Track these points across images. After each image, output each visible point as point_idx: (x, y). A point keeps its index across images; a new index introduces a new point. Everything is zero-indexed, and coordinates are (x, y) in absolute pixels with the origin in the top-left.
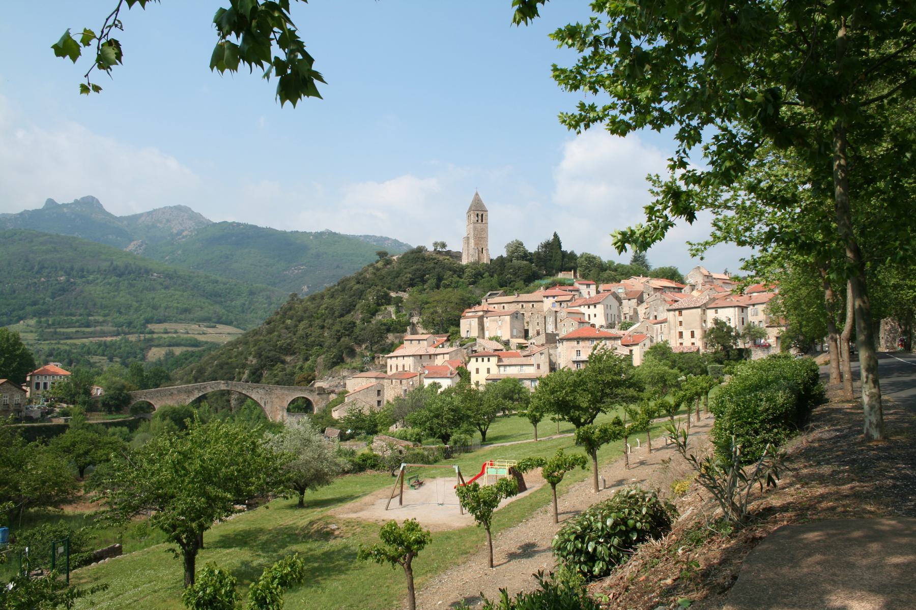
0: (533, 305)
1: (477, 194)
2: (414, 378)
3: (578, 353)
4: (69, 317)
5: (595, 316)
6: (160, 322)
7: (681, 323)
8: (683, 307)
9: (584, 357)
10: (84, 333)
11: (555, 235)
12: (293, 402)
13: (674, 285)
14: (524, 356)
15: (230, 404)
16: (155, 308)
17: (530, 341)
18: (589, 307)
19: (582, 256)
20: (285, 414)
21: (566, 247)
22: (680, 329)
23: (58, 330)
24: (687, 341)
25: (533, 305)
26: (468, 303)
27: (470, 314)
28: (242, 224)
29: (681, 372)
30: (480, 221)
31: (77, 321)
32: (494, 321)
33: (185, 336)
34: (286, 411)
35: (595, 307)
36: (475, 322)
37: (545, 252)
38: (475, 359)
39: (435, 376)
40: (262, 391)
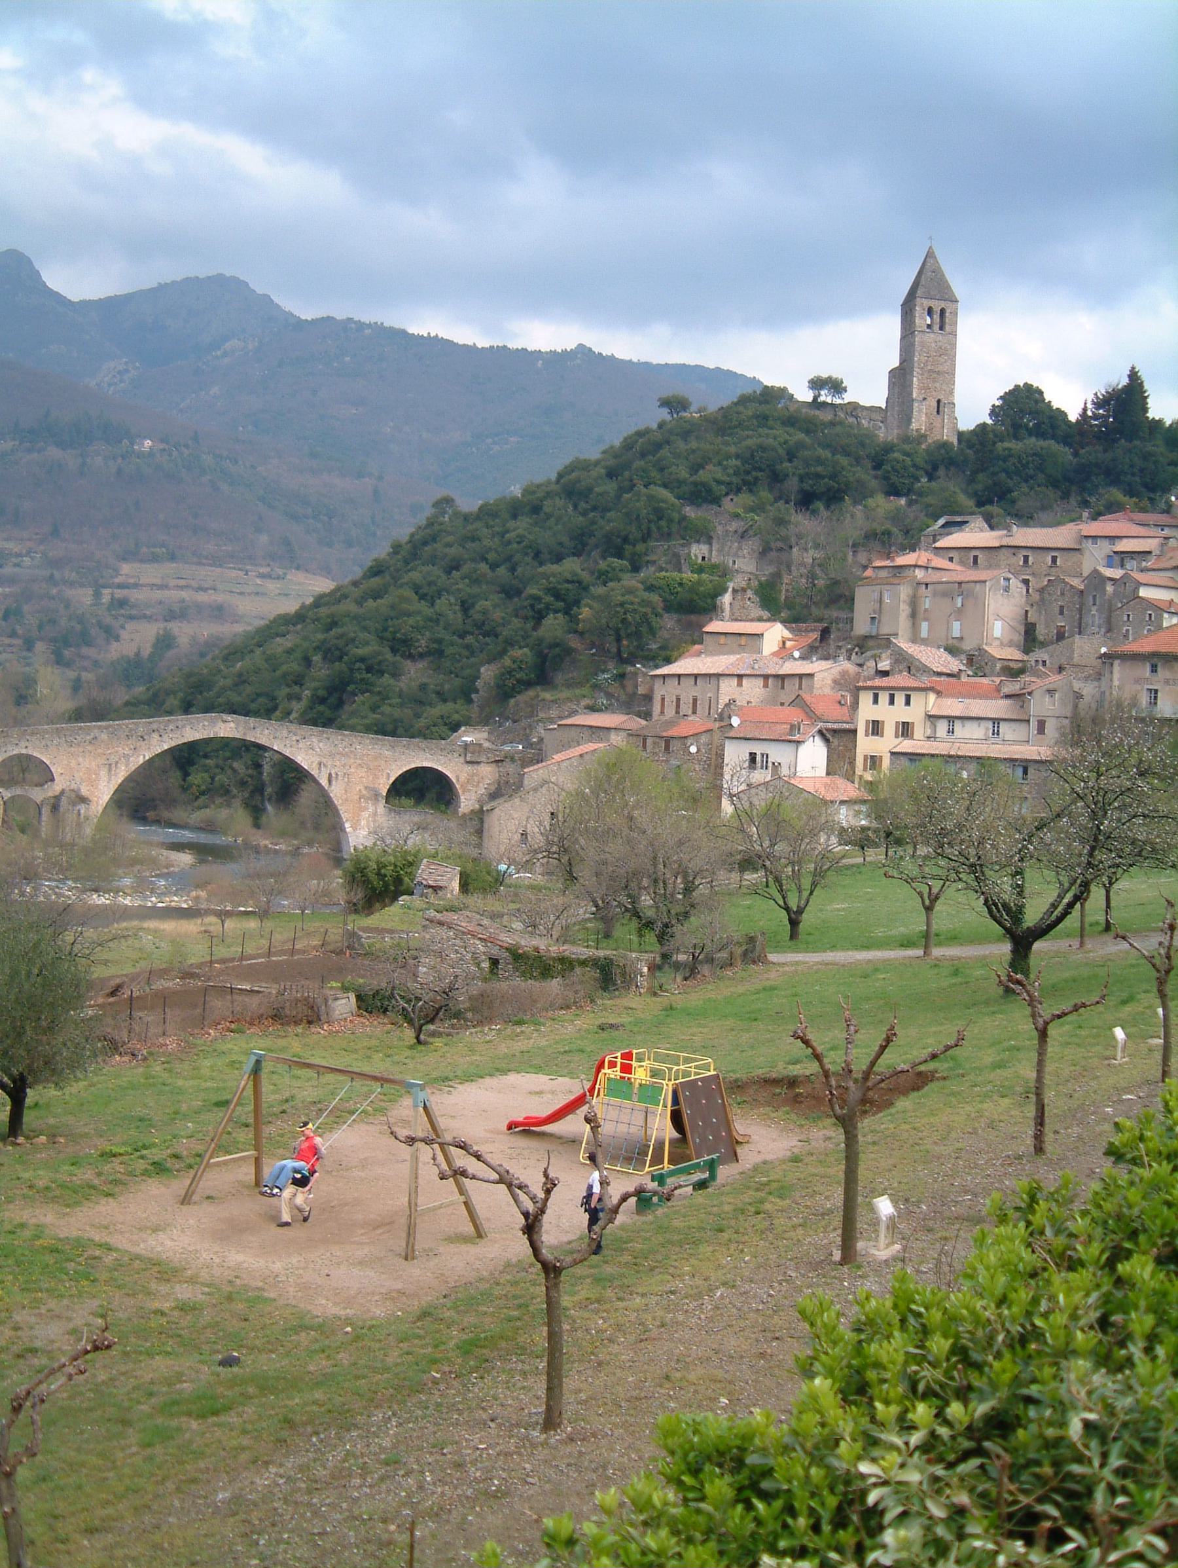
0: (1054, 559)
1: (930, 255)
2: (704, 739)
11: (1133, 375)
15: (261, 773)
20: (381, 807)
25: (1054, 559)
30: (936, 327)
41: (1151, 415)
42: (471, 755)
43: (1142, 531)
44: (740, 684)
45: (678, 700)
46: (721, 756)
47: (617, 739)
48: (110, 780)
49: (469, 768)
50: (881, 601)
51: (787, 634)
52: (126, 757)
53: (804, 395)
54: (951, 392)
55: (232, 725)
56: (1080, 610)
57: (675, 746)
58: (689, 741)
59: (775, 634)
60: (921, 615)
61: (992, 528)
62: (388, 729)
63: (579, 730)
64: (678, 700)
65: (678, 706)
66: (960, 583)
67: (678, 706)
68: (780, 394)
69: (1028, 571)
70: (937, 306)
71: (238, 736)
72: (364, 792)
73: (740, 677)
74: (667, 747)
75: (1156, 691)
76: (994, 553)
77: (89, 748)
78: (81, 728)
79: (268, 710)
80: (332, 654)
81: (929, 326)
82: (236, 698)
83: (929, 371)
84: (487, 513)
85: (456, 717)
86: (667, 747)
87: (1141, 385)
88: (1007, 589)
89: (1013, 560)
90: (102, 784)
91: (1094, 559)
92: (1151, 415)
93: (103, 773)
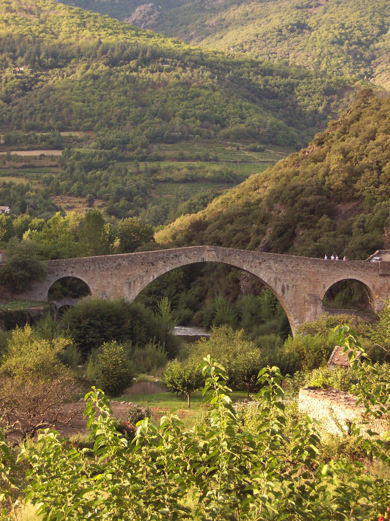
4: (31, 132)
6: (173, 140)
12: (51, 291)
16: (166, 117)
23: (13, 153)
29: (313, 335)
31: (44, 139)
40: (276, 267)
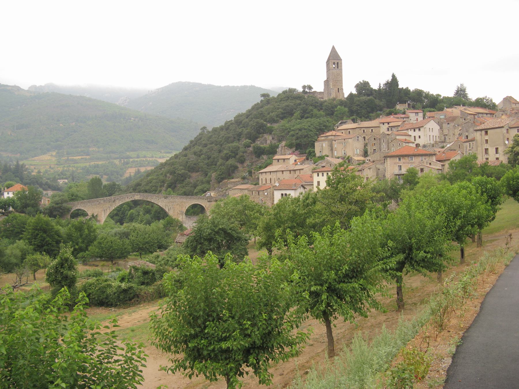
0: (372, 130)
2: (269, 190)
3: (400, 167)
5: (420, 137)
6: (134, 150)
7: (487, 141)
8: (488, 127)
9: (404, 171)
10: (86, 159)
11: (393, 76)
13: (487, 112)
14: (359, 171)
17: (368, 158)
18: (414, 131)
19: (413, 92)
20: (184, 216)
21: (402, 85)
22: (486, 146)
23: (70, 158)
24: (492, 156)
25: (372, 130)
26: (322, 130)
27: (323, 138)
28: (192, 83)
32: (340, 143)
33: (151, 159)
34: (184, 215)
35: (419, 130)
36: (325, 144)
37: (385, 89)
38: (7, 193)
39: (283, 188)
41: (400, 87)
42: (210, 200)
43: (397, 120)
44: (283, 173)
45: (266, 179)
46: (273, 195)
47: (246, 192)
48: (105, 214)
49: (209, 203)
50: (322, 146)
51: (297, 158)
52: (109, 207)
53: (301, 90)
54: (342, 86)
55: (139, 196)
56: (380, 144)
57: (261, 193)
58: (265, 191)
59: (293, 158)
60: (334, 149)
61: (354, 123)
62: (186, 194)
63: (237, 190)
64: (266, 179)
65: (266, 181)
66: (344, 139)
67: (266, 181)
68: (294, 90)
69: (365, 134)
70: (336, 62)
71: (141, 199)
72: (179, 212)
73: (283, 171)
74: (259, 194)
75: (401, 166)
76: (354, 130)
77: (98, 206)
78: (95, 200)
79: (154, 190)
80: (173, 173)
81: (334, 68)
82: (147, 188)
83: (336, 80)
84: (215, 130)
85: (205, 189)
86: (259, 194)
87: (396, 79)
88: (358, 140)
89: (360, 131)
90: (103, 215)
91: (384, 129)
92: (400, 87)
93: (103, 213)
